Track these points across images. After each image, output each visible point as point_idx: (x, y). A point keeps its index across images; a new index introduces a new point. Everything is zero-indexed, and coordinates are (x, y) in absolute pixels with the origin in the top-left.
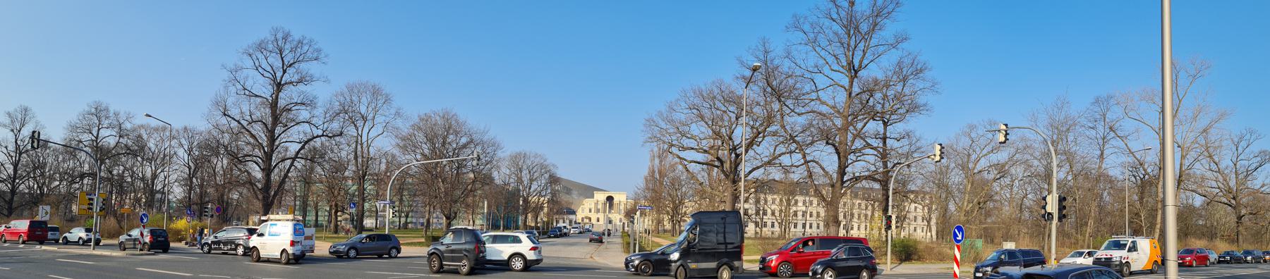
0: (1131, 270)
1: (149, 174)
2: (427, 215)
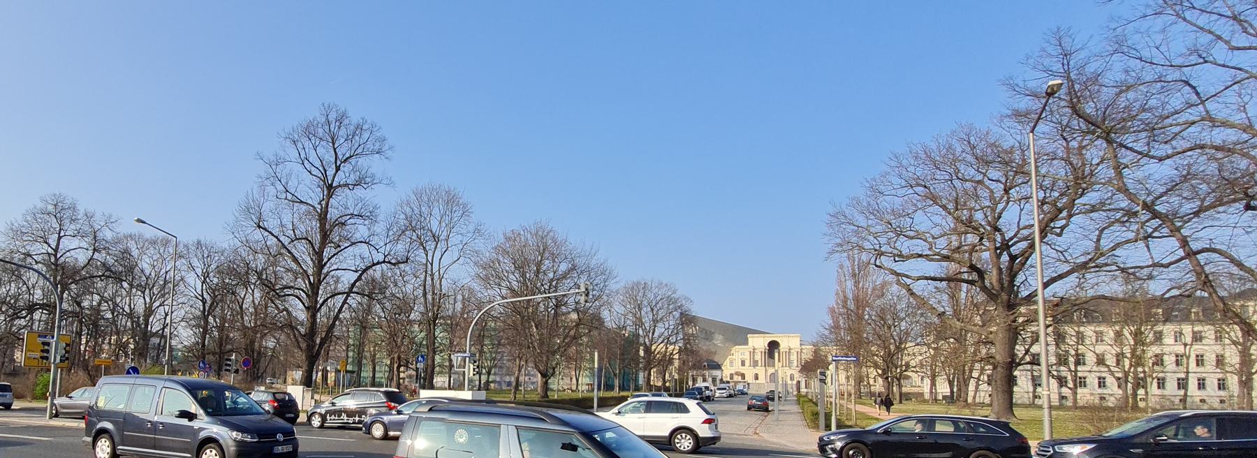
1: (140, 308)
2: (517, 372)
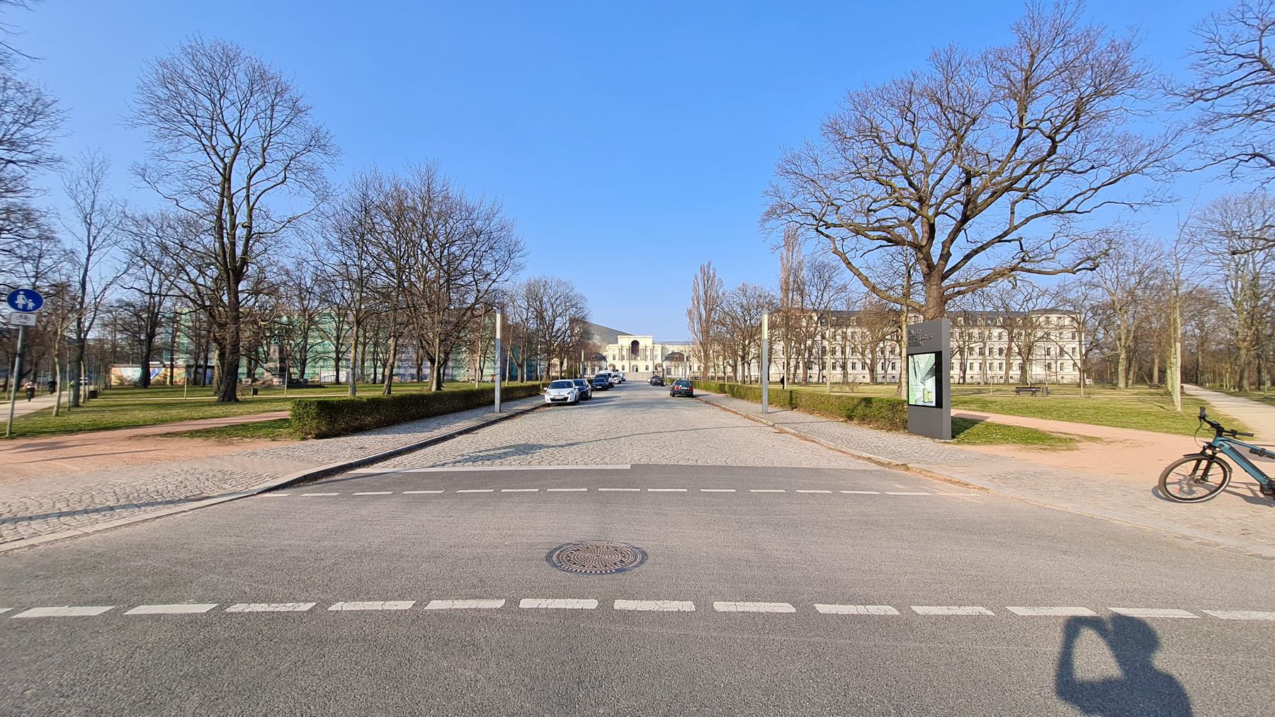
0: (934, 404)
